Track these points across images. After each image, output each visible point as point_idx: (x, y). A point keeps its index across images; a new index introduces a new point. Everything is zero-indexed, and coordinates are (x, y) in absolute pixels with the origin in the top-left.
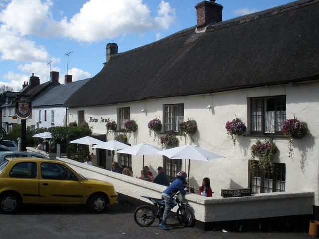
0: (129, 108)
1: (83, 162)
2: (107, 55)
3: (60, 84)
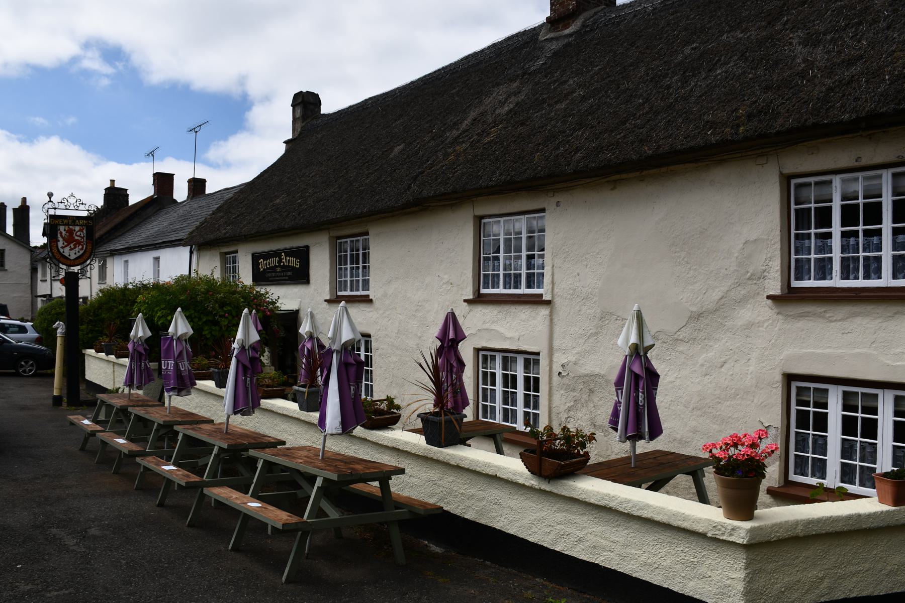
0: (307, 248)
3: (175, 201)
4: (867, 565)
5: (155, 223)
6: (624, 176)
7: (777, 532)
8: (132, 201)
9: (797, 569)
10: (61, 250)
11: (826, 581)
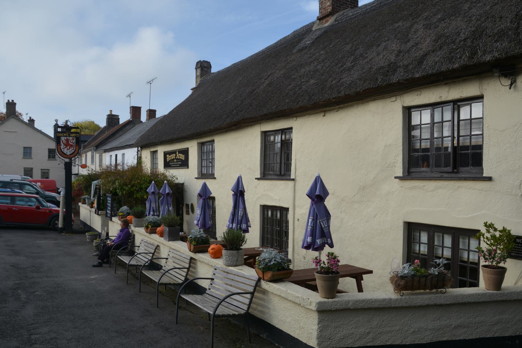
0: (188, 148)
2: (197, 77)
3: (142, 122)
4: (398, 328)
6: (328, 108)
7: (336, 305)
8: (121, 121)
9: (352, 327)
10: (63, 150)
11: (371, 334)
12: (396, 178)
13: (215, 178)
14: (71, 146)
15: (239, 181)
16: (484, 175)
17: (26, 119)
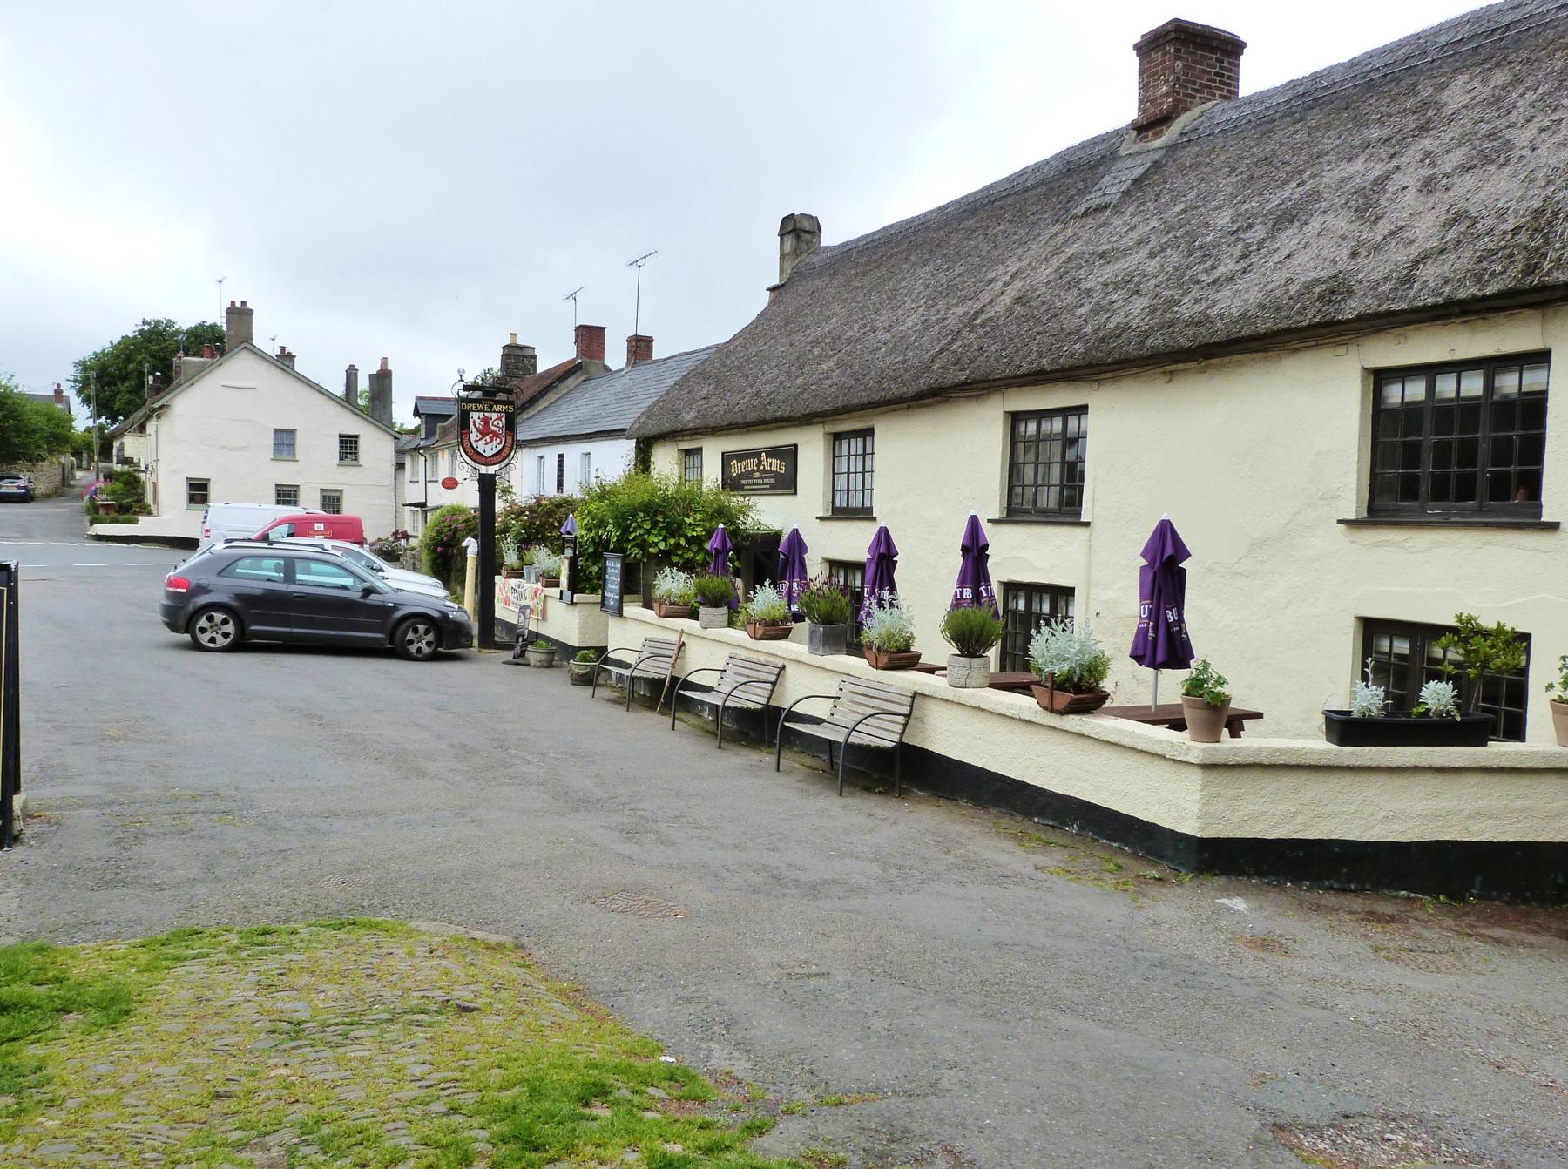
0: (796, 446)
1: (1483, 743)
2: (783, 256)
3: (606, 368)
4: (1353, 808)
5: (580, 402)
6: (1181, 366)
8: (542, 366)
12: (1340, 522)
13: (874, 519)
14: (496, 435)
15: (974, 523)
16: (1543, 519)
17: (273, 351)
